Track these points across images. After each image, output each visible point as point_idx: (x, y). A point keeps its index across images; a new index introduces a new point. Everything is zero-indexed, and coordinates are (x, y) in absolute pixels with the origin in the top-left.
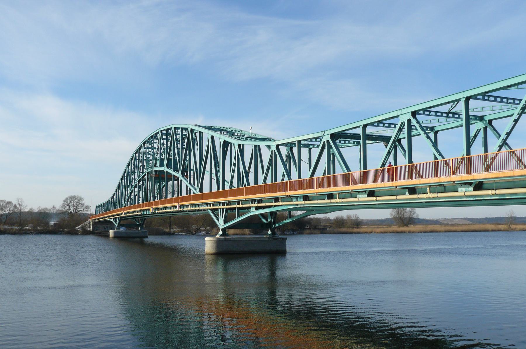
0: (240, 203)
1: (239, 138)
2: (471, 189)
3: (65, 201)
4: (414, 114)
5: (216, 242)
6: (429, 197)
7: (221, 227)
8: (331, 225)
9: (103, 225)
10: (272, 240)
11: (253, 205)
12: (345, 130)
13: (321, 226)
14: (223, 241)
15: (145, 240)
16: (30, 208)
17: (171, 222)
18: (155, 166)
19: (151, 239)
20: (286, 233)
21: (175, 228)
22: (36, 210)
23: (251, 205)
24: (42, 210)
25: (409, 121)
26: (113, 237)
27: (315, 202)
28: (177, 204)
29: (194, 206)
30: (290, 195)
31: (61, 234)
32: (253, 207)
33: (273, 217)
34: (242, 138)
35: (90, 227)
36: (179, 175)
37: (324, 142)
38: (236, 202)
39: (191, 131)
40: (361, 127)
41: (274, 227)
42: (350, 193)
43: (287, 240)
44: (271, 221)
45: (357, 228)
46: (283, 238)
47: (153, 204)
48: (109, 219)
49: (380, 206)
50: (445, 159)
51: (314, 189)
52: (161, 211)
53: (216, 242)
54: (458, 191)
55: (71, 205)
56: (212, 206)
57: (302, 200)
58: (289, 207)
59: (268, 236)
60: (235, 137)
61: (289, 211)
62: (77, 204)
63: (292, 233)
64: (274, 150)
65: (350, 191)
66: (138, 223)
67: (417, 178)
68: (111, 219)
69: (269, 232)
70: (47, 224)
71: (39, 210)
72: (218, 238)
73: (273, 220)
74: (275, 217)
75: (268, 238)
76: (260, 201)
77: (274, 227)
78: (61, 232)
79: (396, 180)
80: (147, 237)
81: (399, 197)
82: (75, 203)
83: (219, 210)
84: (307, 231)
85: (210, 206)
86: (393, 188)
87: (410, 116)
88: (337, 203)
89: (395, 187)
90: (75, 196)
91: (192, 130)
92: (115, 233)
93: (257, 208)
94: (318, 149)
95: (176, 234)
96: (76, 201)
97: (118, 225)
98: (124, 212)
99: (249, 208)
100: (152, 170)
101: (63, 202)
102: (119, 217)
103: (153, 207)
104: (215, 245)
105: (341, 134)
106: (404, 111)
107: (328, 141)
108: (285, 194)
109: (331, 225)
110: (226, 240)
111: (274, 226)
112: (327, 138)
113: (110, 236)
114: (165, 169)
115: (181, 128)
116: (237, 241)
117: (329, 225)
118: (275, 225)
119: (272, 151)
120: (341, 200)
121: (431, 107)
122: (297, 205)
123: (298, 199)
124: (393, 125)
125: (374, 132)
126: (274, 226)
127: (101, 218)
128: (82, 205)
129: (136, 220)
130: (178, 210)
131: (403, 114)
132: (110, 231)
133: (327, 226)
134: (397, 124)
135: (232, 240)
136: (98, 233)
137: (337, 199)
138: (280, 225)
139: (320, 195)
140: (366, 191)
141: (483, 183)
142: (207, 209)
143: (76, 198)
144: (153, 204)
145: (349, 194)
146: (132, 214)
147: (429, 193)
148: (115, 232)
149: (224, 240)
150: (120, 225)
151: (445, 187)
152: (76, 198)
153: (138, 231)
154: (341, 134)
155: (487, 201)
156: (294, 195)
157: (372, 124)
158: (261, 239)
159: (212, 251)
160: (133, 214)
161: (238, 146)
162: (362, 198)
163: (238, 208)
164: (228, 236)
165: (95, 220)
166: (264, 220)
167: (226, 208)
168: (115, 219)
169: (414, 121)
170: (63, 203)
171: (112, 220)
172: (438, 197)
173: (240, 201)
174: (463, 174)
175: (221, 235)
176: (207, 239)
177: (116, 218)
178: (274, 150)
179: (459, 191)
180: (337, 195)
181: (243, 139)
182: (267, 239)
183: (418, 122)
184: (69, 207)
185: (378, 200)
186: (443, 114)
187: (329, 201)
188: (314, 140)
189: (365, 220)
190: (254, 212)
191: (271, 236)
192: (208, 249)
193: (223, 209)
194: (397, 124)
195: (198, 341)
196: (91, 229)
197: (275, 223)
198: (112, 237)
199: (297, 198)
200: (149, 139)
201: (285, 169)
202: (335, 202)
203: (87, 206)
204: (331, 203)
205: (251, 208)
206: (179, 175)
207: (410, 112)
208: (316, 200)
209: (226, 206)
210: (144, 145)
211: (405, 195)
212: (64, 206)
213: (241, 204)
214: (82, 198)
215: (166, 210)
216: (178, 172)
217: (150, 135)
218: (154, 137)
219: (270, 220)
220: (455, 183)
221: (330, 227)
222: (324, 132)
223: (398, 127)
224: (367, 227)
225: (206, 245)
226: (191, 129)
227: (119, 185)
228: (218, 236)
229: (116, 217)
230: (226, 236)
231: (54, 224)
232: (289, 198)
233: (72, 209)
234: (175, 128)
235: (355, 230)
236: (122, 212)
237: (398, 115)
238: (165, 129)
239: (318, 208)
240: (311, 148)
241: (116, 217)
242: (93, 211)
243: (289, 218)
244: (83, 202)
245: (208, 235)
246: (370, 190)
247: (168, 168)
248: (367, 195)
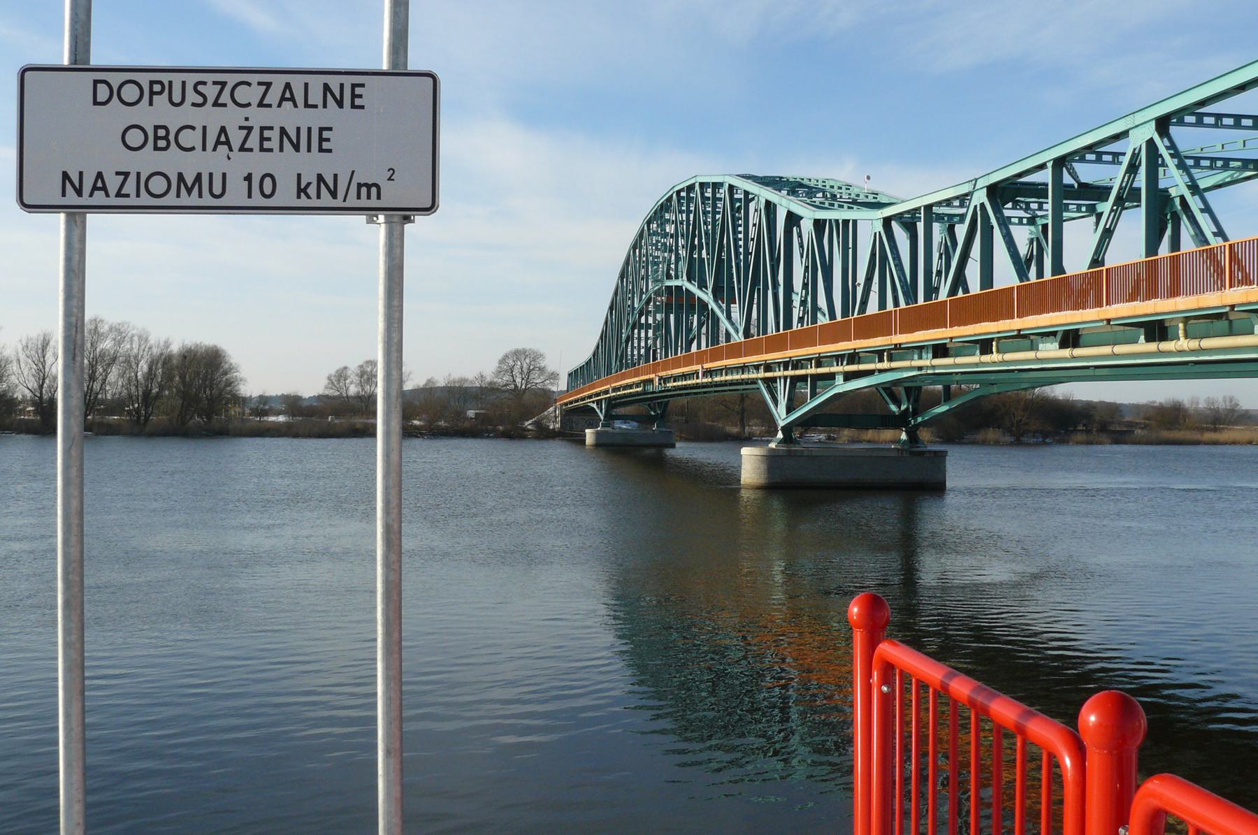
0: (994, 349)
1: (824, 203)
2: (1056, 345)
3: (503, 361)
4: (1163, 124)
5: (765, 458)
6: (1181, 349)
7: (781, 424)
8: (1147, 422)
9: (587, 418)
10: (908, 455)
11: (840, 369)
12: (1020, 175)
13: (1120, 423)
14: (783, 456)
15: (669, 452)
16: (429, 378)
17: (743, 410)
18: (669, 277)
19: (682, 451)
20: (1024, 439)
21: (756, 426)
22: (441, 383)
23: (834, 369)
24: (454, 382)
25: (1151, 143)
26: (593, 446)
27: (1106, 350)
28: (698, 367)
29: (729, 371)
30: (900, 344)
31: (488, 437)
32: (838, 373)
33: (911, 400)
34: (830, 204)
35: (555, 422)
36: (707, 297)
37: (976, 207)
38: (1142, 330)
39: (728, 190)
40: (1050, 165)
41: (913, 423)
42: (1227, 319)
43: (947, 458)
44: (907, 409)
45: (1215, 430)
46: (935, 452)
47: (660, 367)
48: (590, 402)
49: (1098, 372)
50: (1210, 245)
51: (947, 328)
52: (729, 378)
53: (765, 458)
54: (1253, 334)
55: (516, 371)
56: (888, 360)
57: (930, 355)
58: (906, 375)
59: (899, 447)
60: (815, 202)
61: (946, 384)
62: (529, 369)
63: (1041, 440)
64: (880, 232)
65: (1227, 309)
66: (652, 413)
67: (1218, 290)
68: (593, 402)
69: (904, 436)
70: (460, 414)
71: (448, 383)
72: (772, 450)
73: (911, 407)
74: (916, 401)
75: (899, 449)
76: (853, 357)
77: (913, 423)
78: (488, 432)
79: (1107, 305)
80: (673, 446)
81: (1119, 349)
82: (525, 366)
83: (778, 380)
84: (1080, 437)
85: (698, 378)
86: (1101, 324)
87: (1150, 131)
88: (1181, 352)
89: (1105, 322)
90: (523, 349)
91: (731, 187)
92: (598, 435)
93: (849, 377)
94: (962, 225)
95: (755, 438)
96: (528, 361)
97: (605, 417)
98: (612, 385)
99: (831, 376)
100: (662, 286)
101: (497, 365)
102: (606, 399)
103: (660, 374)
104: (763, 467)
105: (1022, 187)
106: (1140, 118)
107: (982, 205)
108: (889, 343)
109: (1147, 422)
110: (790, 454)
111: (912, 421)
112: (980, 197)
113: (587, 444)
114: (683, 282)
115: (713, 183)
116: (817, 456)
117: (1142, 421)
118: (916, 421)
119: (875, 233)
120: (1194, 344)
121: (1202, 103)
122: (920, 368)
123: (923, 354)
124: (1251, 121)
125: (1202, 149)
126: (912, 421)
127: (577, 401)
128: (542, 370)
129: (649, 405)
130: (699, 381)
131: (1137, 126)
132: (587, 431)
133: (1137, 423)
134: (1124, 154)
135: (806, 454)
136: (572, 435)
137: (995, 353)
138: (926, 418)
139: (961, 344)
140: (1057, 331)
141: (1080, 333)
142: (756, 379)
143: (527, 353)
144: (660, 367)
145: (1223, 324)
146: (680, 383)
147: (1182, 339)
148: (598, 434)
149: (785, 454)
150: (610, 417)
151: (1231, 322)
152: (527, 353)
153: (652, 432)
154: (1022, 187)
155: (1197, 366)
156: (975, 335)
157: (1080, 155)
158: (881, 454)
159: (755, 481)
160: (684, 383)
161: (814, 225)
162: (1046, 350)
163: (812, 376)
164: (797, 445)
165: (566, 404)
166: (893, 408)
167: (792, 378)
168: (599, 403)
169: (1161, 145)
170: (499, 367)
171: (594, 406)
172: (1038, 359)
173: (992, 339)
174: (1183, 294)
175: (780, 442)
176: (746, 451)
177: (601, 400)
178: (880, 232)
179: (1256, 332)
180: (1181, 325)
181: (833, 205)
182: (894, 454)
183: (1172, 146)
184: (512, 376)
185: (1007, 362)
186: (1243, 120)
187: (1152, 347)
188: (957, 203)
189: (1137, 408)
190: (841, 386)
191: (906, 447)
192: (748, 475)
193: (786, 378)
194: (1124, 154)
195: (1009, 811)
196: (558, 426)
197: (916, 414)
198: (591, 445)
199: (921, 352)
200: (655, 213)
201: (902, 278)
202: (990, 361)
203: (552, 374)
204: (1161, 353)
205: (837, 377)
206: (707, 297)
207: (1152, 120)
208: (1110, 345)
209: (790, 373)
210: (649, 229)
211: (1137, 343)
212: (499, 372)
213: (998, 351)
214: (541, 355)
215: (743, 374)
216: (707, 289)
217: (658, 202)
218: (665, 207)
219: (905, 406)
220: (1236, 309)
221: (1145, 427)
222: (974, 182)
223: (1126, 160)
224: (1243, 430)
225: (743, 467)
226: (729, 185)
227: (606, 323)
228: (773, 445)
229: (599, 398)
230: (792, 445)
231: (476, 413)
232: (896, 352)
233: (518, 380)
234: (702, 185)
235: (1209, 436)
236: (609, 386)
237: (1127, 128)
238: (684, 188)
239: (993, 377)
240: (954, 225)
241: (599, 398)
242: (562, 385)
243: (945, 401)
244: (543, 365)
245: (831, 441)
246: (1066, 330)
247: (689, 280)
248: (1059, 344)
